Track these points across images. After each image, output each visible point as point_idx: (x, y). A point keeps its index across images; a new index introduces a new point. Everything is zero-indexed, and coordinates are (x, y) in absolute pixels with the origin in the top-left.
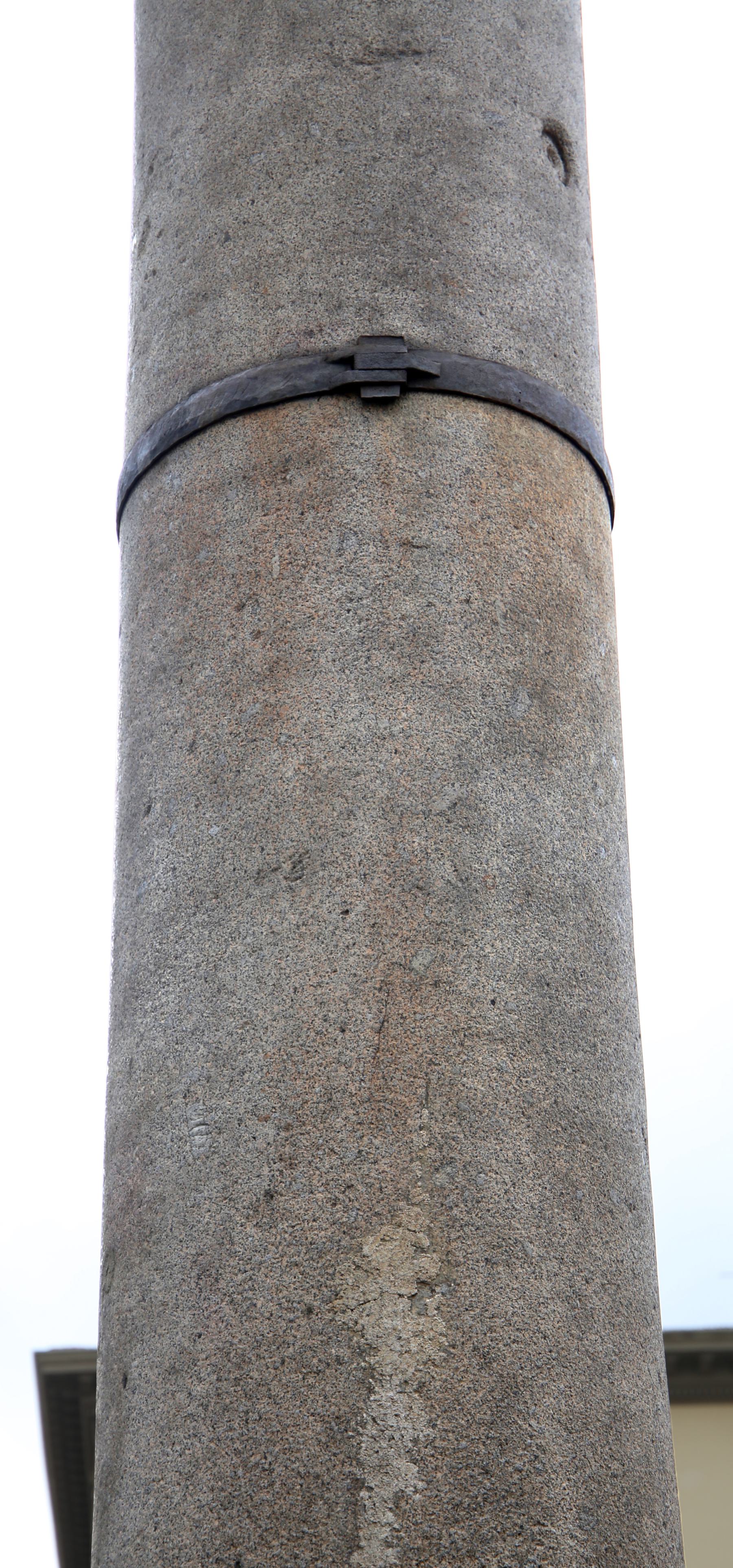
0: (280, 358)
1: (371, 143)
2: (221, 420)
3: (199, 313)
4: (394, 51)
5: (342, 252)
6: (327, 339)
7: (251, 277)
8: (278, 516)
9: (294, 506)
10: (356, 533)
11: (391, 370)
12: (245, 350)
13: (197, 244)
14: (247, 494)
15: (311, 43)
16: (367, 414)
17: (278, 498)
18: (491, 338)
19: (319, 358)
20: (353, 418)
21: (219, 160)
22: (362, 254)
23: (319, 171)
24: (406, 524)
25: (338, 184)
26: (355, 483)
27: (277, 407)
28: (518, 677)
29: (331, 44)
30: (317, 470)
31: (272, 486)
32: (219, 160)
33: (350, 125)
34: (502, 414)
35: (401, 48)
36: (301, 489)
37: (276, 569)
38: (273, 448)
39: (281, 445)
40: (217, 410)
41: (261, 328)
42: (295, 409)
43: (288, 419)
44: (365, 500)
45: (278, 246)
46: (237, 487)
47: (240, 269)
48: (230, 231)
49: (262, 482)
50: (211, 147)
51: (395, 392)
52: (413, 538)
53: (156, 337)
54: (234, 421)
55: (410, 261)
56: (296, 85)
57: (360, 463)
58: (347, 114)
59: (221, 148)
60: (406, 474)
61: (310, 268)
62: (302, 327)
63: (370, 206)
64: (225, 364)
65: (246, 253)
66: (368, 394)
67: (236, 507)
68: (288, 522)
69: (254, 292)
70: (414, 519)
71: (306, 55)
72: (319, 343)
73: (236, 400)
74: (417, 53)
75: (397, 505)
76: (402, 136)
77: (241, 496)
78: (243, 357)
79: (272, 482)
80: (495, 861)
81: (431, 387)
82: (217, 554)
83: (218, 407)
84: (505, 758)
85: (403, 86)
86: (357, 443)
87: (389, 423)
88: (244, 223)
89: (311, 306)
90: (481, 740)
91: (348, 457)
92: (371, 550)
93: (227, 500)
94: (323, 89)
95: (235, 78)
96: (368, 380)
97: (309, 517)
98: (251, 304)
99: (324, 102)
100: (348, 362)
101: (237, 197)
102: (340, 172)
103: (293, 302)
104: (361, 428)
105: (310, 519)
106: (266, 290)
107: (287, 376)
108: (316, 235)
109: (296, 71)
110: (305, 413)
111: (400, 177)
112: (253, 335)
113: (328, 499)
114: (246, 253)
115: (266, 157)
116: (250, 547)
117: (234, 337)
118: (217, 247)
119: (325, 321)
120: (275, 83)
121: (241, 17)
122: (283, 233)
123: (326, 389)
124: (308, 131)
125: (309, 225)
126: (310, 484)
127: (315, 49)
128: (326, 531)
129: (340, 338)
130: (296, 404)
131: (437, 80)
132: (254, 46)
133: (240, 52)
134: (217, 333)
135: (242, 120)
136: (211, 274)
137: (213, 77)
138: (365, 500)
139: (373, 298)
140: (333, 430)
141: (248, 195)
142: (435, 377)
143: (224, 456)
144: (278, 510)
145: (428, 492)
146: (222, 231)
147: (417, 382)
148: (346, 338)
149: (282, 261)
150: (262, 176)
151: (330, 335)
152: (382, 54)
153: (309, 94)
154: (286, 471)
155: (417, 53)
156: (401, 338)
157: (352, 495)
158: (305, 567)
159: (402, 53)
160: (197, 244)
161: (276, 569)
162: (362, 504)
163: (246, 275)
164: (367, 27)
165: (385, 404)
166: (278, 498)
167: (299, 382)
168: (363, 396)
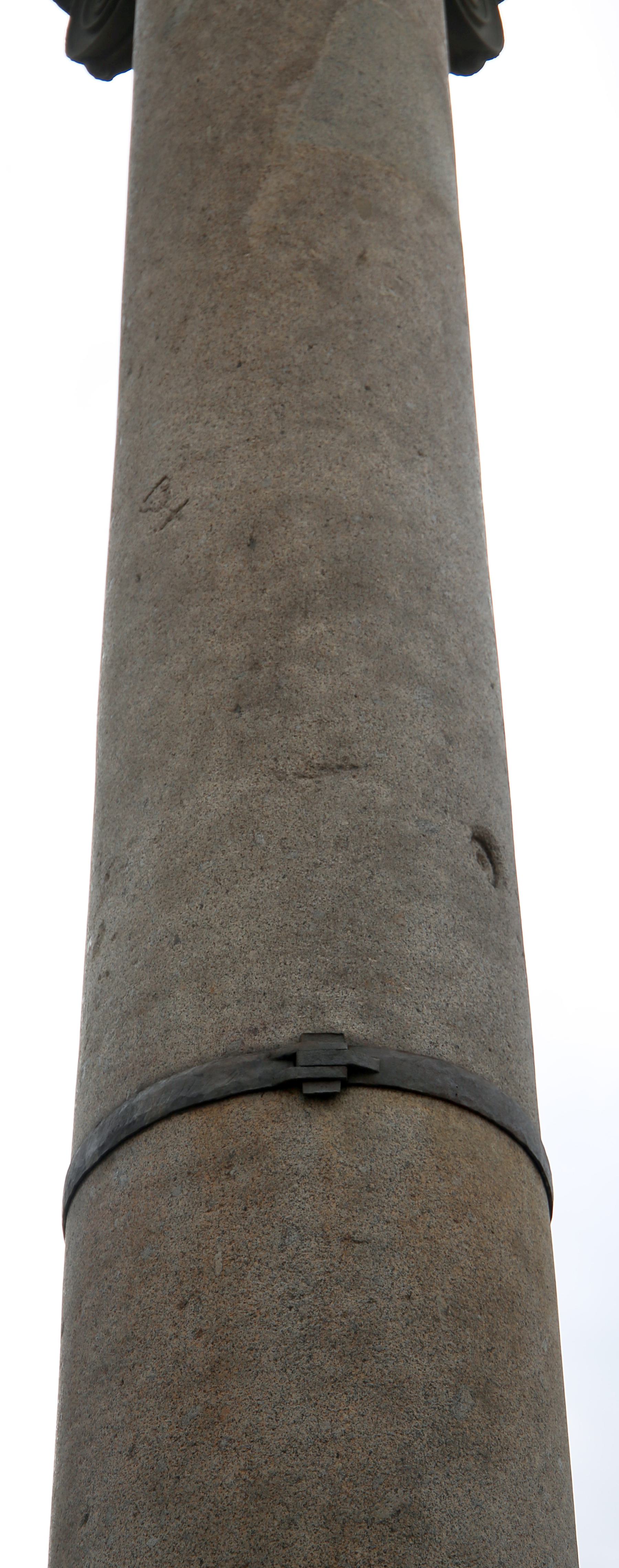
1: (313, 850)
3: (149, 1013)
6: (270, 1036)
7: (198, 978)
8: (221, 1212)
9: (237, 1201)
10: (298, 1228)
11: (332, 1066)
12: (192, 1048)
13: (148, 946)
16: (309, 1109)
19: (263, 1055)
21: (171, 867)
24: (347, 1219)
25: (281, 888)
26: (297, 1178)
27: (222, 1104)
29: (275, 759)
30: (261, 1165)
31: (216, 1182)
32: (171, 867)
35: (339, 763)
36: (244, 1184)
37: (219, 1265)
38: (218, 1144)
39: (225, 1141)
41: (208, 1026)
42: (240, 1105)
43: (232, 1115)
44: (307, 1195)
47: (188, 970)
49: (207, 1178)
55: (349, 960)
57: (302, 1158)
58: (290, 824)
59: (173, 856)
60: (347, 1169)
63: (311, 909)
64: (173, 1062)
65: (195, 955)
66: (309, 1089)
69: (201, 992)
70: (355, 1214)
71: (253, 770)
72: (263, 1040)
74: (354, 767)
75: (338, 1200)
77: (186, 1192)
82: (161, 1251)
86: (299, 1138)
89: (256, 1004)
91: (290, 1152)
92: (313, 1246)
96: (310, 1076)
97: (252, 1212)
98: (198, 1003)
99: (269, 813)
100: (290, 1058)
101: (187, 901)
102: (284, 877)
104: (303, 1123)
105: (253, 1215)
108: (261, 937)
109: (243, 785)
110: (249, 1109)
111: (340, 881)
112: (200, 1033)
113: (271, 1194)
114: (195, 955)
115: (214, 864)
116: (193, 1243)
121: (194, 737)
122: (230, 935)
123: (269, 1085)
124: (254, 839)
126: (253, 1179)
130: (240, 1100)
134: (166, 1031)
138: (307, 1195)
141: (197, 900)
144: (222, 1205)
146: (172, 934)
147: (357, 1077)
148: (289, 1035)
149: (228, 962)
150: (211, 882)
152: (322, 768)
154: (230, 1167)
155: (354, 767)
156: (342, 1034)
157: (294, 1190)
158: (247, 1263)
159: (340, 767)
160: (148, 946)
161: (219, 1265)
162: (304, 1199)
163: (194, 976)
164: (308, 744)
165: (326, 1099)
166: (222, 1194)
167: (243, 1079)
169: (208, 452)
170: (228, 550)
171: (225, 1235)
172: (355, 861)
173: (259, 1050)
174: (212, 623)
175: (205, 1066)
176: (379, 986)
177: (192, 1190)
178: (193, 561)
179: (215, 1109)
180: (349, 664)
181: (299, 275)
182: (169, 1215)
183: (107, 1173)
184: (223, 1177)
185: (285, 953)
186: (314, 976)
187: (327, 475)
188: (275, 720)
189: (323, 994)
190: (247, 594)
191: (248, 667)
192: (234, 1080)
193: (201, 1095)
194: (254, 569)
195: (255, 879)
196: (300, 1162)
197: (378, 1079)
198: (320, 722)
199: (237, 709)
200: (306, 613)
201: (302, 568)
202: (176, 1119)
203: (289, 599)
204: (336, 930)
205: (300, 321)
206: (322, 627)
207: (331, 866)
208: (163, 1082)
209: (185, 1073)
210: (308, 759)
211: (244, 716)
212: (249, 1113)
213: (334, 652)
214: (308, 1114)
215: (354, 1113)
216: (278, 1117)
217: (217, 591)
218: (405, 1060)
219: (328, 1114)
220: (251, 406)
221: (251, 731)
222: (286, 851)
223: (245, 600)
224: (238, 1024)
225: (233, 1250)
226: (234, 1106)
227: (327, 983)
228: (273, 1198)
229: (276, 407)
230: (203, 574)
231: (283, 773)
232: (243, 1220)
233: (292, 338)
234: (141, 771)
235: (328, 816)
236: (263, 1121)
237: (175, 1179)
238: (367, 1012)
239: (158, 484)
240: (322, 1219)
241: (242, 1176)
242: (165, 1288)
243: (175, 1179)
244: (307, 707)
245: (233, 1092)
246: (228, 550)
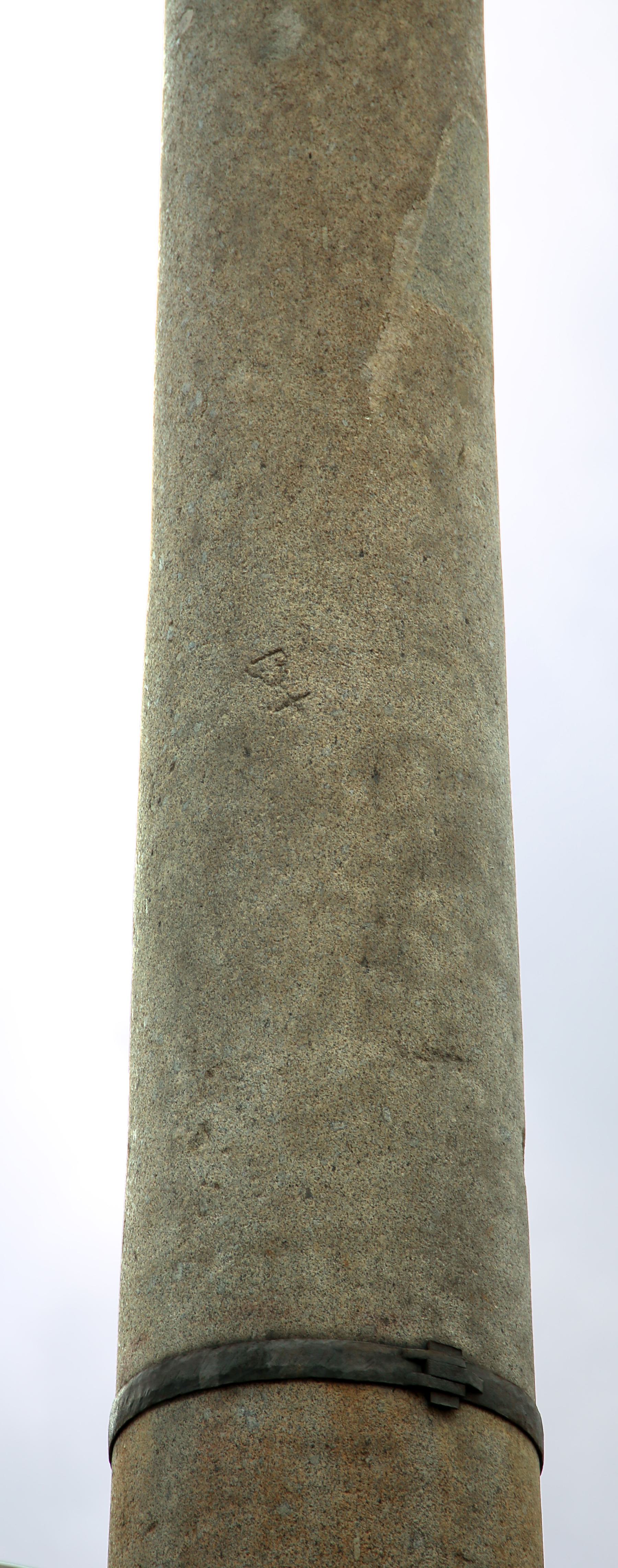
0: (360, 1337)
1: (431, 1142)
2: (304, 1378)
3: (278, 1258)
4: (444, 1053)
5: (410, 1247)
6: (399, 1331)
7: (332, 1244)
8: (359, 1496)
9: (373, 1491)
10: (423, 1535)
11: (455, 1382)
12: (327, 1316)
13: (276, 1185)
14: (330, 1465)
15: (384, 1027)
16: (431, 1417)
17: (359, 1479)
19: (396, 1350)
20: (421, 1418)
21: (300, 1111)
22: (427, 1254)
23: (391, 1159)
24: (459, 1536)
25: (406, 1176)
26: (422, 1484)
27: (359, 1387)
29: (399, 1032)
30: (393, 1461)
31: (353, 1465)
32: (300, 1111)
33: (414, 1120)
35: (448, 1051)
36: (379, 1476)
37: (357, 1551)
38: (355, 1426)
39: (361, 1426)
40: (302, 1369)
41: (343, 1300)
42: (374, 1394)
43: (367, 1402)
44: (430, 1503)
45: (357, 1222)
46: (319, 1453)
47: (322, 1232)
48: (312, 1188)
49: (344, 1457)
50: (292, 1094)
52: (464, 1550)
53: (221, 1255)
54: (317, 1385)
55: (459, 1270)
56: (372, 1065)
57: (426, 1465)
58: (412, 1108)
59: (302, 1100)
60: (459, 1485)
61: (386, 1255)
62: (379, 1312)
63: (430, 1206)
64: (308, 1323)
65: (328, 1218)
66: (436, 1400)
67: (319, 1473)
68: (368, 1506)
69: (335, 1261)
70: (465, 1532)
71: (380, 1037)
72: (392, 1333)
73: (322, 1367)
74: (459, 1059)
75: (453, 1515)
76: (452, 1141)
77: (324, 1465)
78: (325, 1323)
79: (353, 1460)
82: (300, 1515)
83: (301, 1366)
85: (451, 1091)
86: (424, 1444)
87: (446, 1431)
88: (326, 1186)
89: (387, 1293)
91: (417, 1456)
92: (434, 1555)
93: (309, 1463)
94: (394, 1076)
95: (316, 1034)
96: (438, 1387)
97: (386, 1507)
98: (333, 1272)
99: (395, 1090)
100: (422, 1364)
101: (318, 1157)
102: (408, 1165)
103: (371, 1284)
104: (427, 1430)
105: (386, 1510)
106: (347, 1264)
107: (369, 1360)
108: (390, 1223)
109: (372, 1050)
110: (383, 1401)
111: (451, 1182)
112: (335, 1304)
113: (402, 1493)
114: (328, 1218)
115: (346, 1127)
116: (333, 1519)
117: (316, 1299)
118: (298, 1199)
119: (398, 1312)
120: (354, 1056)
121: (320, 976)
122: (361, 1210)
123: (401, 1383)
124: (381, 1114)
125: (383, 1211)
126: (386, 1473)
127: (387, 1033)
128: (399, 1526)
129: (411, 1333)
130: (375, 1389)
131: (473, 1091)
132: (334, 1009)
133: (321, 1010)
134: (299, 1287)
135: (323, 1081)
136: (292, 1224)
137: (292, 1024)
138: (430, 1503)
139: (434, 1300)
140: (406, 1426)
141: (330, 1160)
143: (307, 1417)
144: (358, 1490)
145: (473, 1506)
146: (303, 1186)
147: (471, 1396)
148: (415, 1335)
149: (361, 1239)
150: (343, 1145)
151: (402, 1328)
152: (435, 1053)
153: (382, 1078)
154: (366, 1454)
155: (459, 1059)
156: (460, 1350)
157: (420, 1496)
158: (382, 1557)
159: (448, 1056)
160: (276, 1185)
161: (357, 1551)
162: (428, 1506)
163: (328, 1241)
164: (425, 1025)
165: (445, 1412)
166: (359, 1479)
167: (380, 1370)
168: (432, 1401)
169: (331, 646)
170: (354, 774)
171: (363, 1522)
172: (462, 1164)
173: (392, 1344)
174: (339, 852)
175: (344, 1342)
176: (479, 1301)
177: (330, 1465)
178: (317, 770)
179: (351, 1390)
180: (456, 944)
181: (415, 464)
182: (307, 1482)
183: (229, 1404)
184: (360, 1462)
185: (410, 1247)
186: (433, 1279)
187: (439, 718)
188: (398, 988)
189: (441, 1300)
190: (372, 834)
191: (374, 919)
192: (371, 1368)
193: (340, 1372)
194: (378, 808)
195: (383, 1158)
196: (425, 1468)
197: (482, 1400)
198: (435, 1002)
199: (364, 962)
200: (423, 874)
201: (420, 822)
202: (313, 1386)
203: (409, 854)
204: (450, 1235)
205: (415, 523)
206: (436, 896)
207: (445, 1164)
208: (299, 1342)
209: (323, 1342)
210: (425, 1040)
211: (371, 973)
212: (383, 1405)
213: (445, 927)
214: (431, 1422)
215: (463, 1430)
216: (407, 1417)
217: (342, 818)
218: (498, 1385)
219: (446, 1425)
220: (375, 610)
221: (377, 992)
222: (410, 1136)
223: (371, 841)
224: (371, 1309)
225: (369, 1539)
226: (369, 1393)
227: (443, 1289)
228: (403, 1497)
229: (397, 621)
230: (328, 791)
231: (405, 1049)
232: (378, 1512)
233: (410, 541)
234: (258, 983)
235: (441, 1108)
236: (394, 1417)
237: (313, 1447)
238: (473, 1327)
239: (271, 653)
240: (441, 1531)
241: (376, 1468)
242: (305, 1554)
243: (313, 1447)
244: (425, 983)
245: (370, 1380)
246: (354, 774)
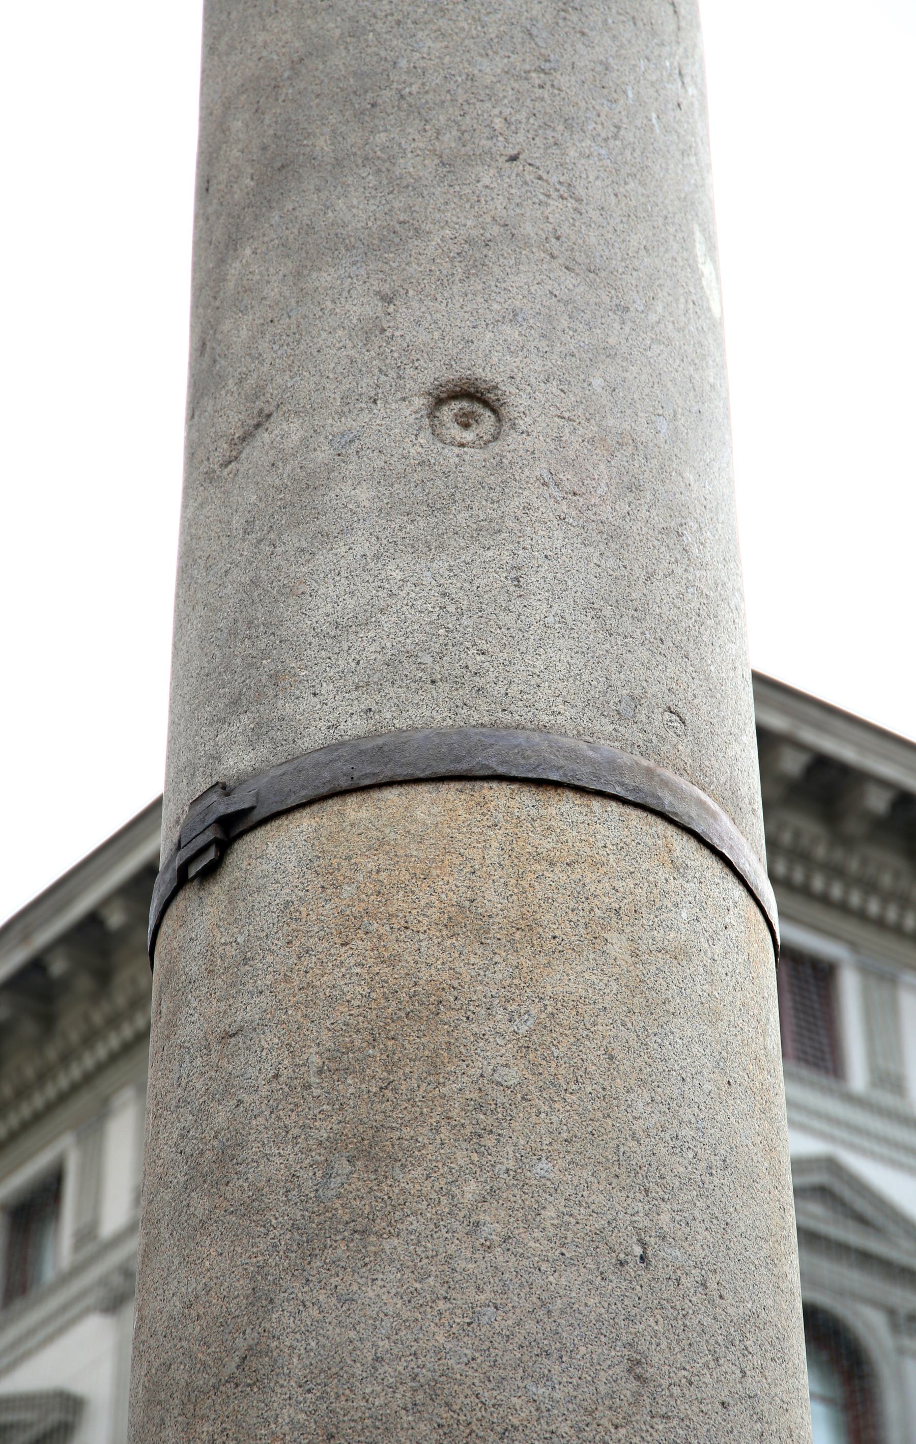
18: (544, 689)
28: (334, 1144)
34: (334, 805)
51: (211, 855)
80: (287, 1413)
81: (250, 824)
84: (309, 1263)
90: (281, 1253)
142: (252, 809)
